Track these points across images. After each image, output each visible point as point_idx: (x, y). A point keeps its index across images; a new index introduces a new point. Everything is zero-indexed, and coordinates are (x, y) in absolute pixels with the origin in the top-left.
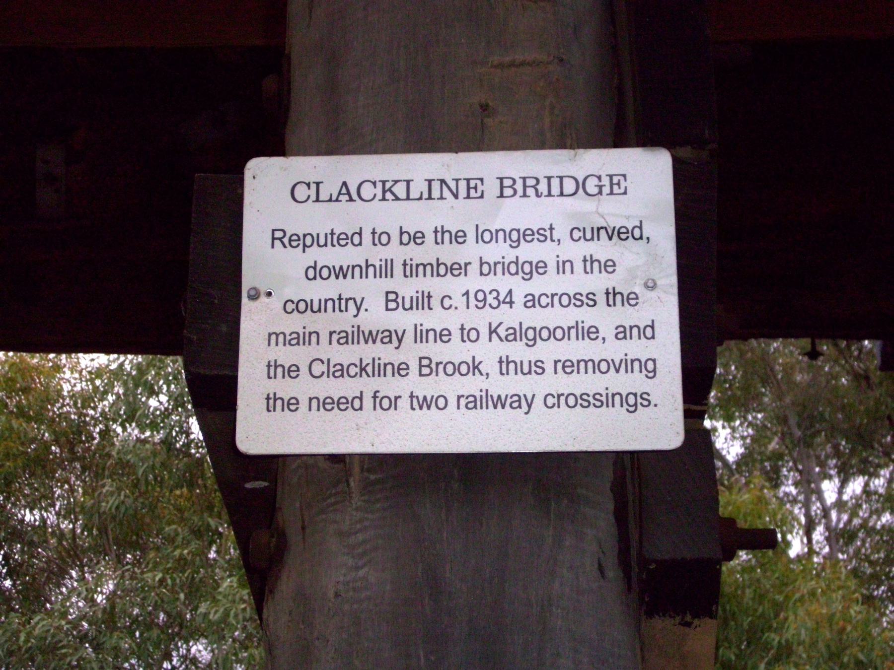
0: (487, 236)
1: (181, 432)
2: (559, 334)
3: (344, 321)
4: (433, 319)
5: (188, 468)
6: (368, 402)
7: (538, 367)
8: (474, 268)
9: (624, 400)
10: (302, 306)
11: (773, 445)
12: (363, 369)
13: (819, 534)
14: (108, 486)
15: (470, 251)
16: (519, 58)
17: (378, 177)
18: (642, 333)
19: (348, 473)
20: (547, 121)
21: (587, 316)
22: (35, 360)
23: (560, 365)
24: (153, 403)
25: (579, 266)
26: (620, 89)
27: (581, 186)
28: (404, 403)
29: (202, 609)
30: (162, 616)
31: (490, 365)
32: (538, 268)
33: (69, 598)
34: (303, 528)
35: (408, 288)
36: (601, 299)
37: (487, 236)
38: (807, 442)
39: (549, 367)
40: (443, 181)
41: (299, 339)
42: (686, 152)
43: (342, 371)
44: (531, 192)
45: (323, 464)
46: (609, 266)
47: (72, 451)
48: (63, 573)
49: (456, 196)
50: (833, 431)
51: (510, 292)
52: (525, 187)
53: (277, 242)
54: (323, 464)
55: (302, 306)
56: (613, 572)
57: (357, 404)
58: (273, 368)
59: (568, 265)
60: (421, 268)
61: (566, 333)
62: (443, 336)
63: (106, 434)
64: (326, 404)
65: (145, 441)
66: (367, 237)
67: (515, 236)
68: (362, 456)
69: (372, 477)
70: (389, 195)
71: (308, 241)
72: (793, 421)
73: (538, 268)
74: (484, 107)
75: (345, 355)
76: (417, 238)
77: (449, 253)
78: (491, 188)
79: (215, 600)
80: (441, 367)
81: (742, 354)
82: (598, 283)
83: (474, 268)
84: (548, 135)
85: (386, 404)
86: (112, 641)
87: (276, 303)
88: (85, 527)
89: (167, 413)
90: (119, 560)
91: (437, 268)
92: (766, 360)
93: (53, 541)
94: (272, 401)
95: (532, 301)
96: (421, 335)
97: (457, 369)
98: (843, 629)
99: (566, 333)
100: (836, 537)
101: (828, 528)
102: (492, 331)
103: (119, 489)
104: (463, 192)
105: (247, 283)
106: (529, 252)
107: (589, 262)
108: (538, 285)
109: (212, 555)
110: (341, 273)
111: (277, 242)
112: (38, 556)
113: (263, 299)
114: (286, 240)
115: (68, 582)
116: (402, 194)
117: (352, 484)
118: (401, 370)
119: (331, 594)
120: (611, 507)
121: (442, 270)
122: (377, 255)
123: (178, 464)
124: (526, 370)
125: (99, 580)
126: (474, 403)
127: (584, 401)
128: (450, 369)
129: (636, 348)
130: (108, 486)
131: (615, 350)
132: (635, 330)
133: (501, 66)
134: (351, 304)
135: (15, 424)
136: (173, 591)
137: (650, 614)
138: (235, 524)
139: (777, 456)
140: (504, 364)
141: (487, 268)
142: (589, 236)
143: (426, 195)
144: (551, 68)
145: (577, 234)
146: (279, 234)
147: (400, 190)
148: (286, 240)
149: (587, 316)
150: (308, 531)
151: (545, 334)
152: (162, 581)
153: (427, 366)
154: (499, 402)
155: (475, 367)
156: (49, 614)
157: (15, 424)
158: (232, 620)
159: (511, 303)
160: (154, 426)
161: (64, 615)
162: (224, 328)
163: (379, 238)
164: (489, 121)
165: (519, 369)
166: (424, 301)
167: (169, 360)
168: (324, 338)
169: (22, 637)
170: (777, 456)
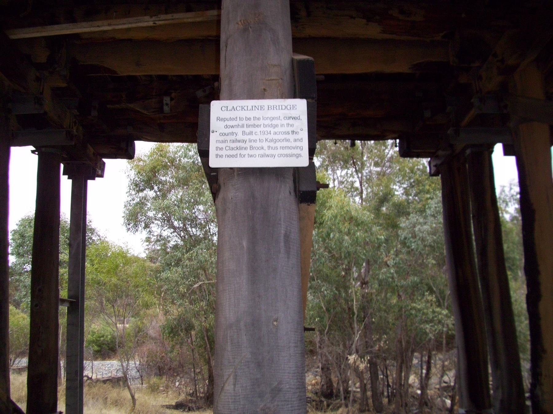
0: (265, 119)
1: (197, 160)
2: (281, 140)
3: (233, 138)
4: (253, 137)
5: (198, 168)
6: (238, 156)
7: (276, 148)
8: (262, 126)
10: (224, 134)
11: (327, 163)
12: (237, 148)
13: (336, 182)
14: (180, 172)
15: (261, 122)
16: (272, 78)
17: (241, 105)
18: (299, 140)
19: (234, 172)
20: (279, 93)
21: (287, 137)
22: (164, 144)
24: (190, 153)
25: (286, 125)
26: (295, 86)
27: (286, 107)
28: (247, 156)
29: (201, 198)
30: (192, 200)
31: (266, 147)
32: (276, 126)
33: (172, 196)
35: (247, 130)
36: (291, 133)
37: (265, 119)
38: (334, 162)
39: (279, 148)
41: (224, 142)
42: (310, 100)
43: (233, 149)
44: (275, 109)
45: (228, 169)
46: (292, 125)
47: (172, 164)
48: (170, 191)
50: (339, 160)
54: (229, 170)
55: (224, 134)
56: (293, 194)
57: (236, 156)
61: (283, 140)
62: (255, 141)
63: (180, 160)
64: (229, 156)
65: (188, 162)
66: (238, 119)
67: (297, 155)
68: (237, 168)
71: (225, 119)
72: (331, 158)
73: (276, 126)
74: (264, 89)
76: (249, 119)
77: (257, 122)
78: (266, 108)
79: (204, 196)
81: (320, 143)
82: (290, 129)
83: (262, 126)
85: (242, 156)
86: (182, 205)
87: (218, 133)
88: (175, 181)
89: (193, 156)
90: (183, 188)
91: (254, 126)
92: (325, 145)
93: (168, 184)
94: (217, 156)
95: (275, 133)
96: (250, 141)
97: (258, 148)
98: (344, 203)
99: (283, 140)
100: (341, 183)
101: (338, 181)
102: (266, 140)
104: (260, 108)
105: (212, 128)
106: (275, 122)
107: (288, 125)
108: (277, 130)
109: (203, 187)
110: (232, 127)
112: (165, 187)
113: (215, 132)
115: (172, 193)
116: (246, 109)
119: (230, 198)
120: (292, 179)
121: (255, 126)
122: (240, 123)
123: (196, 167)
125: (179, 192)
126: (262, 156)
127: (286, 156)
128: (257, 148)
129: (298, 144)
130: (180, 172)
131: (294, 144)
133: (268, 80)
135: (160, 158)
136: (195, 194)
137: (301, 202)
138: (208, 180)
139: (327, 166)
140: (269, 147)
141: (265, 126)
145: (285, 118)
146: (218, 118)
147: (246, 108)
149: (287, 137)
151: (278, 141)
152: (193, 192)
153: (252, 148)
154: (268, 156)
156: (168, 200)
157: (160, 158)
158: (208, 201)
160: (190, 158)
161: (171, 200)
162: (206, 139)
163: (241, 119)
164: (265, 93)
165: (272, 148)
166: (251, 133)
167: (194, 144)
168: (229, 141)
169: (162, 205)
170: (327, 166)
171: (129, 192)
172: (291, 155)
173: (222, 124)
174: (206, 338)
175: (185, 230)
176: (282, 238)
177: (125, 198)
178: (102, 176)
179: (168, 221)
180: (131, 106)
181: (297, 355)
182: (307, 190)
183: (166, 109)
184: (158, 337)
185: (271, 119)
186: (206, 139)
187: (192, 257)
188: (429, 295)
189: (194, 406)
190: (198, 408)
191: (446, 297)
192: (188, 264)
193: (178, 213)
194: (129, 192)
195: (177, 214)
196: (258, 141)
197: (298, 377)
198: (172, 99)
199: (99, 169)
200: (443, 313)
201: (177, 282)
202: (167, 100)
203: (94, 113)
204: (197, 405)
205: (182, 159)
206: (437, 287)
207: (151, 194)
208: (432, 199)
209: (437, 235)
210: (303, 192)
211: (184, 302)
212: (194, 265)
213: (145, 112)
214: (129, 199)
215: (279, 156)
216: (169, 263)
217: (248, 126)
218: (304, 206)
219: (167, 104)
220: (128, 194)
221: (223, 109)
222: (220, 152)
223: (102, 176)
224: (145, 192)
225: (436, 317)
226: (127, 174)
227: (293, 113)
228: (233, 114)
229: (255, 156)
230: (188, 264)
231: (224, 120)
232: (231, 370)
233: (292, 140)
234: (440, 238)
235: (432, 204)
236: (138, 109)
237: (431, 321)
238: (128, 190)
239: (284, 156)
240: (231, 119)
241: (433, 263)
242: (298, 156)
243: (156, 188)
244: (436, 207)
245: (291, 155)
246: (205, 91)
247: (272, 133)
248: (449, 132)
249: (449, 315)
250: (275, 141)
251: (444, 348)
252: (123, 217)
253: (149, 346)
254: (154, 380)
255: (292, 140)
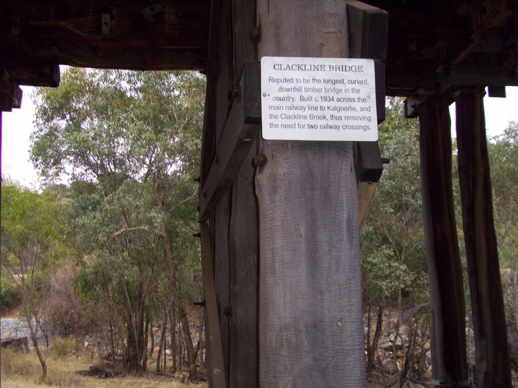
0: (326, 82)
6: (297, 126)
7: (340, 118)
8: (323, 90)
9: (363, 128)
16: (330, 30)
17: (297, 64)
18: (367, 110)
23: (346, 118)
28: (306, 127)
34: (273, 156)
36: (356, 100)
39: (343, 118)
40: (314, 66)
41: (278, 108)
42: (377, 60)
43: (290, 117)
44: (337, 70)
46: (358, 91)
49: (318, 70)
51: (333, 97)
52: (336, 68)
53: (271, 81)
58: (271, 116)
59: (348, 91)
60: (309, 90)
61: (348, 109)
63: (98, 84)
64: (285, 126)
69: (294, 145)
70: (300, 69)
71: (279, 81)
75: (290, 113)
80: (315, 117)
84: (338, 52)
94: (271, 125)
95: (339, 100)
99: (348, 109)
103: (103, 100)
107: (353, 89)
110: (288, 90)
111: (271, 81)
113: (267, 96)
114: (273, 80)
116: (303, 68)
117: (289, 146)
118: (305, 117)
121: (315, 90)
124: (337, 119)
126: (325, 127)
128: (318, 118)
129: (366, 114)
131: (360, 114)
132: (365, 109)
133: (326, 33)
134: (291, 99)
137: (362, 180)
142: (353, 82)
143: (310, 69)
144: (338, 33)
145: (350, 82)
146: (271, 79)
147: (303, 67)
148: (273, 80)
150: (274, 157)
151: (342, 109)
154: (331, 127)
155: (324, 117)
159: (333, 100)
162: (257, 104)
163: (298, 81)
164: (323, 48)
165: (336, 118)
171: (36, 121)
172: (358, 127)
173: (276, 86)
174: (127, 293)
175: (102, 166)
176: (344, 225)
177: (32, 129)
178: (18, 107)
179: (83, 157)
180: (62, 23)
181: (361, 358)
182: (373, 168)
183: (105, 29)
184: (63, 289)
185: (334, 82)
186: (257, 104)
187: (113, 200)
188: (386, 248)
189: (112, 371)
190: (117, 374)
191: (404, 249)
192: (109, 209)
193: (98, 149)
194: (36, 121)
195: (96, 150)
196: (319, 108)
197: (363, 384)
198: (112, 18)
199: (16, 99)
200: (401, 269)
201: (95, 229)
202: (106, 18)
203: (16, 31)
204: (116, 370)
205: (101, 83)
206: (393, 238)
207: (63, 124)
208: (390, 138)
209: (396, 180)
210: (368, 170)
211: (104, 253)
212: (115, 209)
213: (79, 32)
214: (36, 129)
215: (344, 127)
216: (84, 206)
217: (307, 90)
218: (365, 184)
219: (106, 24)
220: (35, 124)
221: (276, 67)
222: (275, 121)
223: (18, 107)
224: (55, 121)
225: (393, 272)
226: (33, 99)
227: (359, 77)
228: (289, 74)
229: (316, 127)
230: (109, 209)
231: (277, 81)
232: (289, 378)
233: (358, 109)
234: (399, 183)
235: (391, 145)
236: (71, 29)
237: (386, 277)
238: (35, 120)
239: (349, 127)
240: (286, 80)
241: (390, 212)
242: (365, 128)
243: (68, 117)
244: (395, 148)
245: (358, 127)
246: (152, 9)
247: (335, 99)
248: (438, 70)
249: (408, 270)
250: (340, 109)
251: (400, 306)
252: (29, 151)
253: (55, 300)
254: (60, 340)
255: (358, 109)
